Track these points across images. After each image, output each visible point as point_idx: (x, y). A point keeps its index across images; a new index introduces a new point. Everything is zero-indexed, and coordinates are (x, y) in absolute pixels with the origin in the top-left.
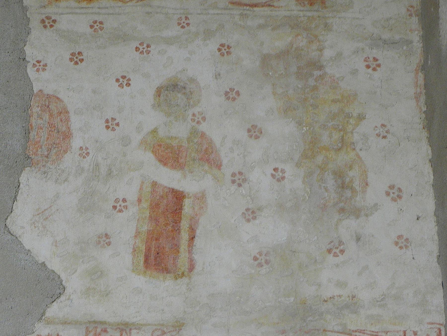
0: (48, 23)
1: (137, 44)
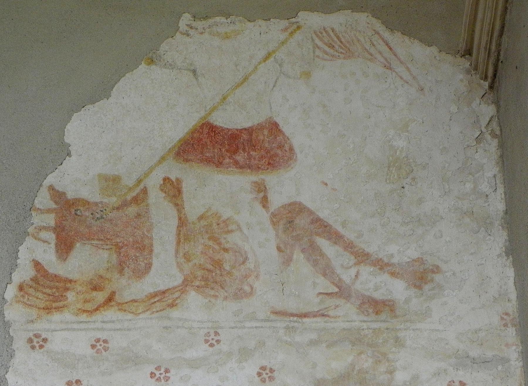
0: (37, 342)
1: (151, 368)
